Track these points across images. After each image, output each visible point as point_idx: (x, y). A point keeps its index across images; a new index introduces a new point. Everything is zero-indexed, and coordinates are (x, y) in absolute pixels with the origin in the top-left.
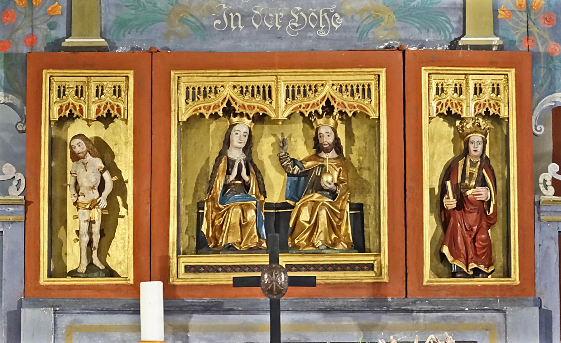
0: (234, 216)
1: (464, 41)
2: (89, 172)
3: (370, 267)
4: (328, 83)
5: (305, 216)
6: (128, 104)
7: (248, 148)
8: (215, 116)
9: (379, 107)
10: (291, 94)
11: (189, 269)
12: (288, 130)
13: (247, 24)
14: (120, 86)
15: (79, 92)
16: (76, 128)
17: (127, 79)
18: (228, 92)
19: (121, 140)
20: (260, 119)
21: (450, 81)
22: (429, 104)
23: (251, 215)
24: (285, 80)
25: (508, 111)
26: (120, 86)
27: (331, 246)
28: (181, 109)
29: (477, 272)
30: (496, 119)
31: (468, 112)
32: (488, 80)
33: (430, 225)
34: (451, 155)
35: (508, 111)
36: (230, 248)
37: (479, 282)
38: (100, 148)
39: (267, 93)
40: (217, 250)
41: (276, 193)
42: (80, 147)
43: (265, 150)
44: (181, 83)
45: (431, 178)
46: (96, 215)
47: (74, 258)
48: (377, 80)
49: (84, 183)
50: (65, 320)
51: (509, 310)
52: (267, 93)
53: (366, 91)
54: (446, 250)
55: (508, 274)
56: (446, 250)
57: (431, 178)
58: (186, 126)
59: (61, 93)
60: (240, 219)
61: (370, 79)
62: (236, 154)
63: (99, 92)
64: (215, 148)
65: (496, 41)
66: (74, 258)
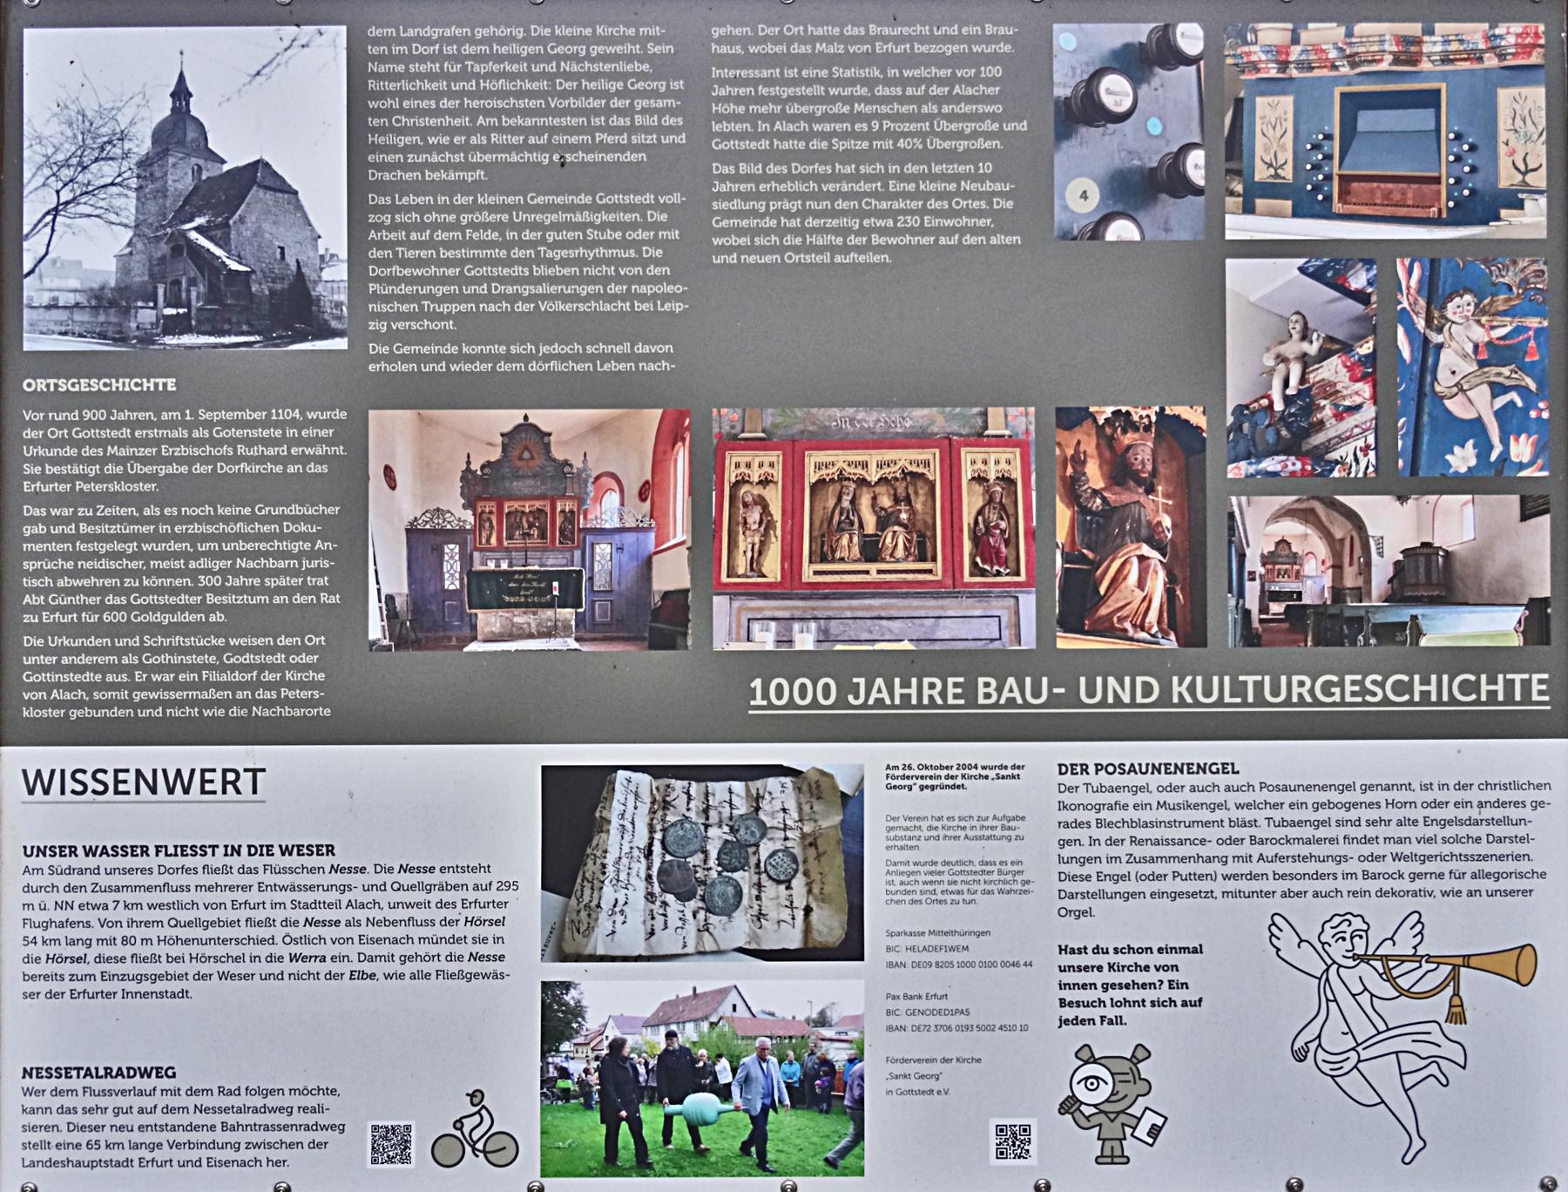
0: (845, 541)
1: (1447, 402)
2: (754, 516)
3: (930, 571)
4: (905, 458)
5: (889, 540)
6: (777, 473)
7: (853, 502)
8: (832, 480)
9: (935, 474)
10: (880, 466)
11: (816, 573)
12: (878, 490)
13: (852, 425)
14: (770, 462)
15: (748, 465)
16: (745, 488)
17: (775, 456)
18: (840, 465)
19: (774, 497)
20: (862, 482)
21: (979, 457)
22: (967, 473)
23: (855, 539)
24: (874, 457)
25: (1017, 474)
26: (770, 462)
27: (906, 559)
28: (811, 476)
29: (998, 574)
30: (1012, 482)
31: (992, 476)
32: (1003, 457)
33: (967, 546)
34: (980, 503)
35: (1017, 474)
36: (842, 560)
37: (999, 579)
38: (762, 502)
39: (865, 465)
40: (833, 561)
41: (870, 528)
42: (749, 499)
43: (865, 502)
44: (812, 459)
45: (967, 519)
46: (757, 540)
47: (742, 565)
48: (932, 455)
49: (750, 520)
50: (736, 604)
51: (1021, 596)
52: (865, 465)
53: (927, 464)
54: (978, 560)
55: (1018, 574)
56: (978, 560)
57: (967, 519)
58: (814, 487)
59: (737, 465)
60: (849, 545)
61: (931, 457)
62: (846, 504)
63: (997, 462)
64: (832, 502)
65: (1007, 432)
66: (742, 565)
